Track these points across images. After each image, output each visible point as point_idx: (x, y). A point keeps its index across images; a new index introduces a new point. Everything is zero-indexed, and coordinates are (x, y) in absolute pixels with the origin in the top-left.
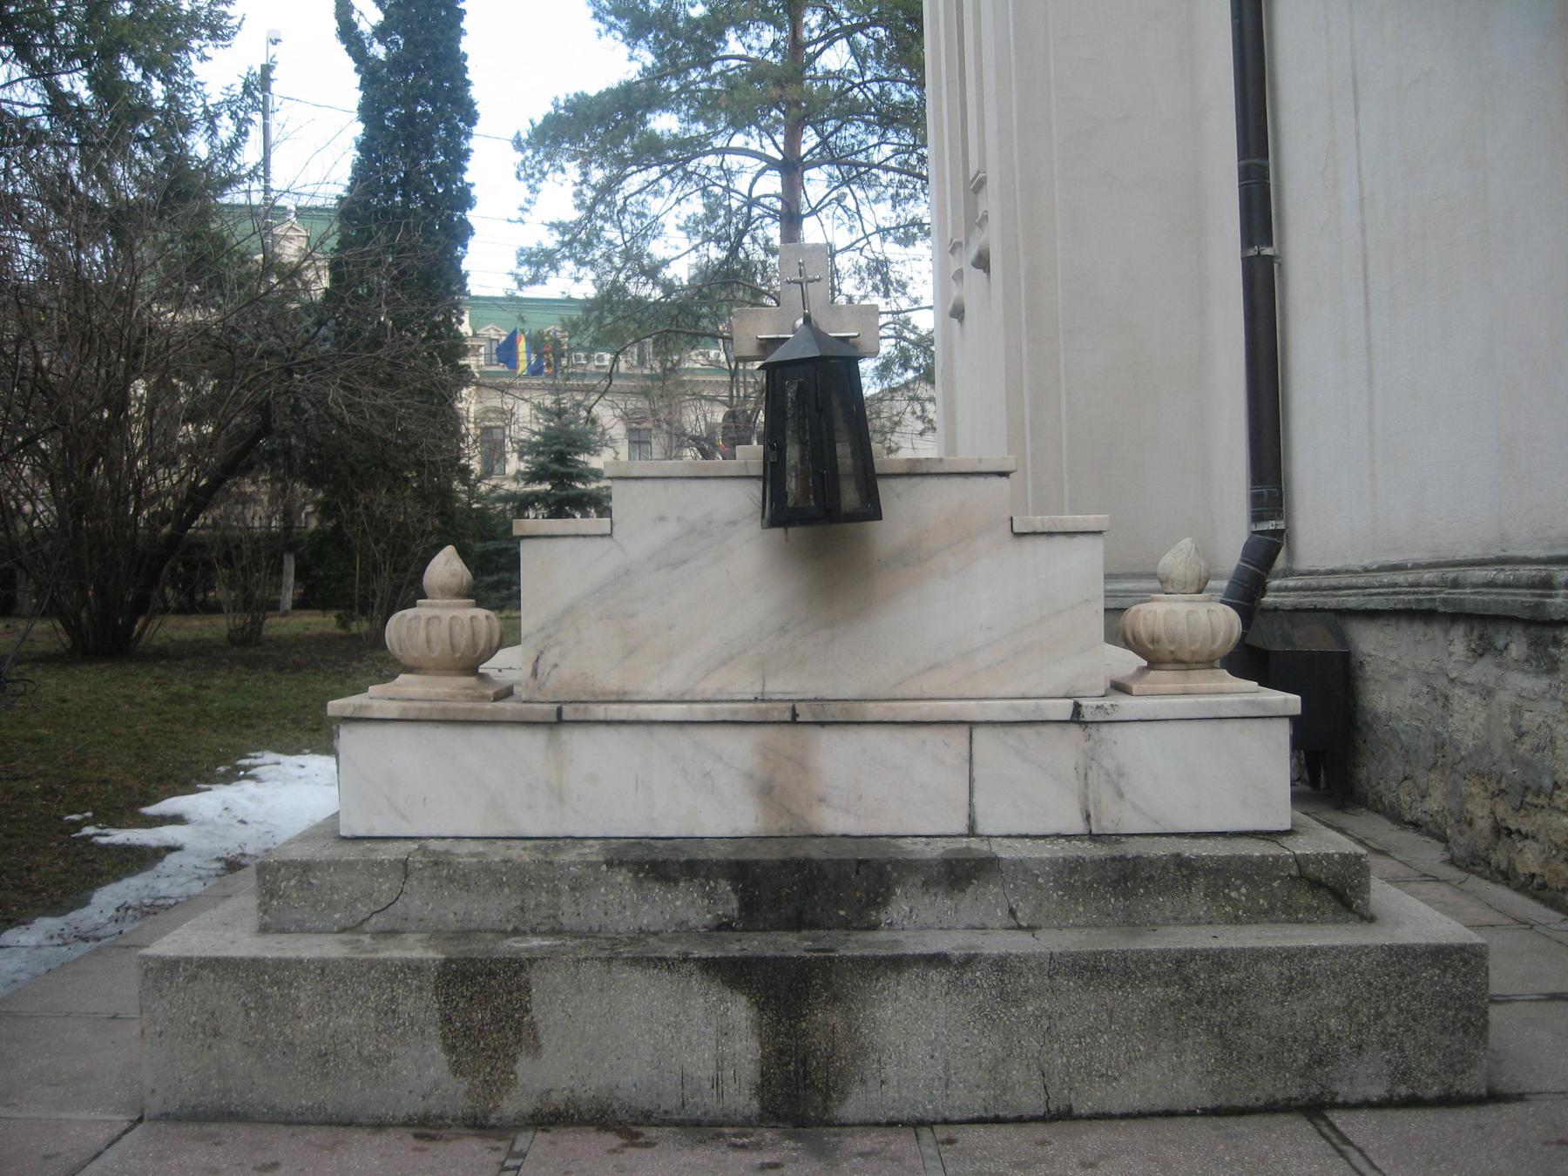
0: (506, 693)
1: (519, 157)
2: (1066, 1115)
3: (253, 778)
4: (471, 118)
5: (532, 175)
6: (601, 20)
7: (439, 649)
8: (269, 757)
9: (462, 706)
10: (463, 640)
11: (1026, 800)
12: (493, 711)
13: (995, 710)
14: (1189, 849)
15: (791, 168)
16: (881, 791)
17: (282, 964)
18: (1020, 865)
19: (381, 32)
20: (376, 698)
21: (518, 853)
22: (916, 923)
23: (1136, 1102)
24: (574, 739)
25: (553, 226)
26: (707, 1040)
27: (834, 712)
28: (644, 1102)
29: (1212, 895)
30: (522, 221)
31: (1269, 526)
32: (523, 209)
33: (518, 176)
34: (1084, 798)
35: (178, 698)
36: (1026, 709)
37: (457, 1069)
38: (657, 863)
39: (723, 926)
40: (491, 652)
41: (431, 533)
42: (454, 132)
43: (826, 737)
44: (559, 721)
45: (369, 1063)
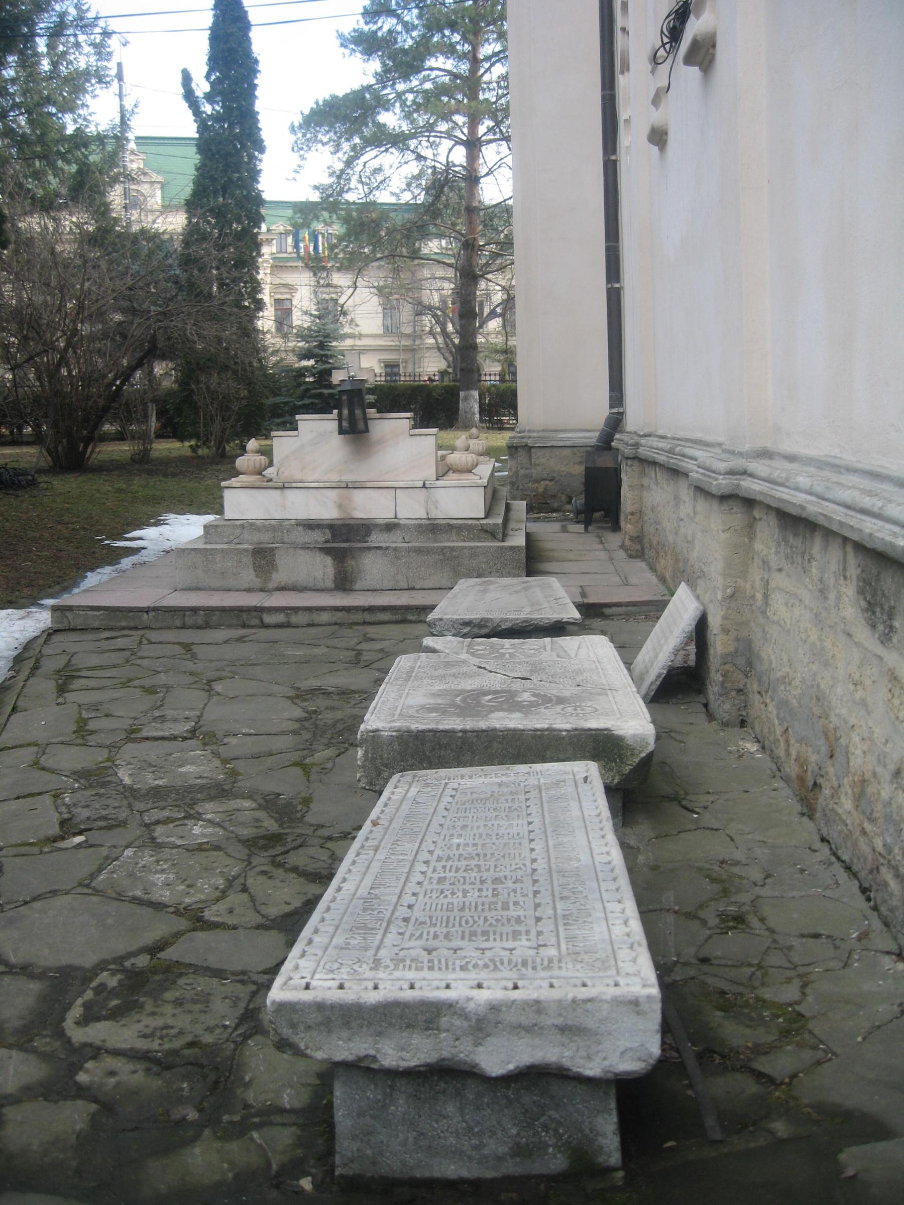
0: (270, 480)
1: (294, 138)
2: (413, 589)
3: (166, 524)
4: (262, 150)
5: (302, 149)
6: (346, 47)
7: (251, 468)
8: (172, 516)
9: (258, 484)
10: (258, 465)
11: (411, 509)
12: (268, 485)
13: (401, 484)
14: (451, 522)
15: (473, 145)
16: (371, 506)
17: (212, 549)
18: (405, 525)
19: (209, 97)
20: (234, 482)
21: (273, 522)
22: (377, 539)
23: (431, 585)
24: (288, 492)
25: (316, 188)
26: (322, 568)
27: (357, 485)
28: (305, 585)
29: (458, 534)
30: (294, 179)
31: (615, 410)
32: (296, 172)
33: (293, 149)
34: (427, 509)
35: (119, 491)
36: (410, 484)
37: (257, 576)
38: (310, 525)
39: (327, 542)
40: (266, 469)
41: (242, 399)
42: (252, 158)
43: (356, 491)
44: (284, 488)
45: (235, 575)
